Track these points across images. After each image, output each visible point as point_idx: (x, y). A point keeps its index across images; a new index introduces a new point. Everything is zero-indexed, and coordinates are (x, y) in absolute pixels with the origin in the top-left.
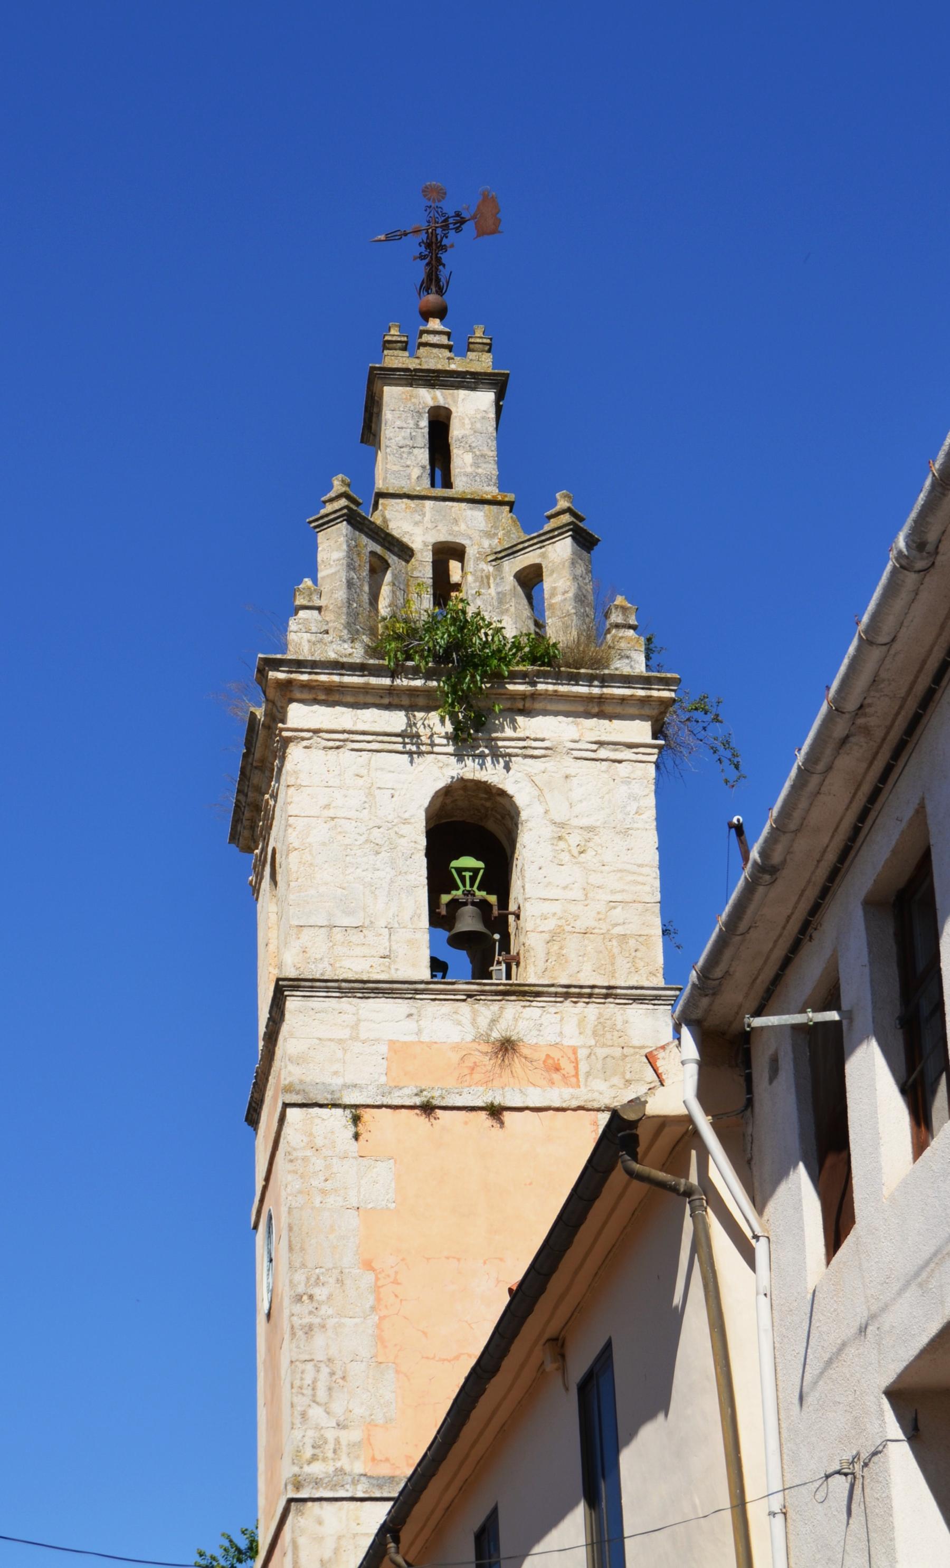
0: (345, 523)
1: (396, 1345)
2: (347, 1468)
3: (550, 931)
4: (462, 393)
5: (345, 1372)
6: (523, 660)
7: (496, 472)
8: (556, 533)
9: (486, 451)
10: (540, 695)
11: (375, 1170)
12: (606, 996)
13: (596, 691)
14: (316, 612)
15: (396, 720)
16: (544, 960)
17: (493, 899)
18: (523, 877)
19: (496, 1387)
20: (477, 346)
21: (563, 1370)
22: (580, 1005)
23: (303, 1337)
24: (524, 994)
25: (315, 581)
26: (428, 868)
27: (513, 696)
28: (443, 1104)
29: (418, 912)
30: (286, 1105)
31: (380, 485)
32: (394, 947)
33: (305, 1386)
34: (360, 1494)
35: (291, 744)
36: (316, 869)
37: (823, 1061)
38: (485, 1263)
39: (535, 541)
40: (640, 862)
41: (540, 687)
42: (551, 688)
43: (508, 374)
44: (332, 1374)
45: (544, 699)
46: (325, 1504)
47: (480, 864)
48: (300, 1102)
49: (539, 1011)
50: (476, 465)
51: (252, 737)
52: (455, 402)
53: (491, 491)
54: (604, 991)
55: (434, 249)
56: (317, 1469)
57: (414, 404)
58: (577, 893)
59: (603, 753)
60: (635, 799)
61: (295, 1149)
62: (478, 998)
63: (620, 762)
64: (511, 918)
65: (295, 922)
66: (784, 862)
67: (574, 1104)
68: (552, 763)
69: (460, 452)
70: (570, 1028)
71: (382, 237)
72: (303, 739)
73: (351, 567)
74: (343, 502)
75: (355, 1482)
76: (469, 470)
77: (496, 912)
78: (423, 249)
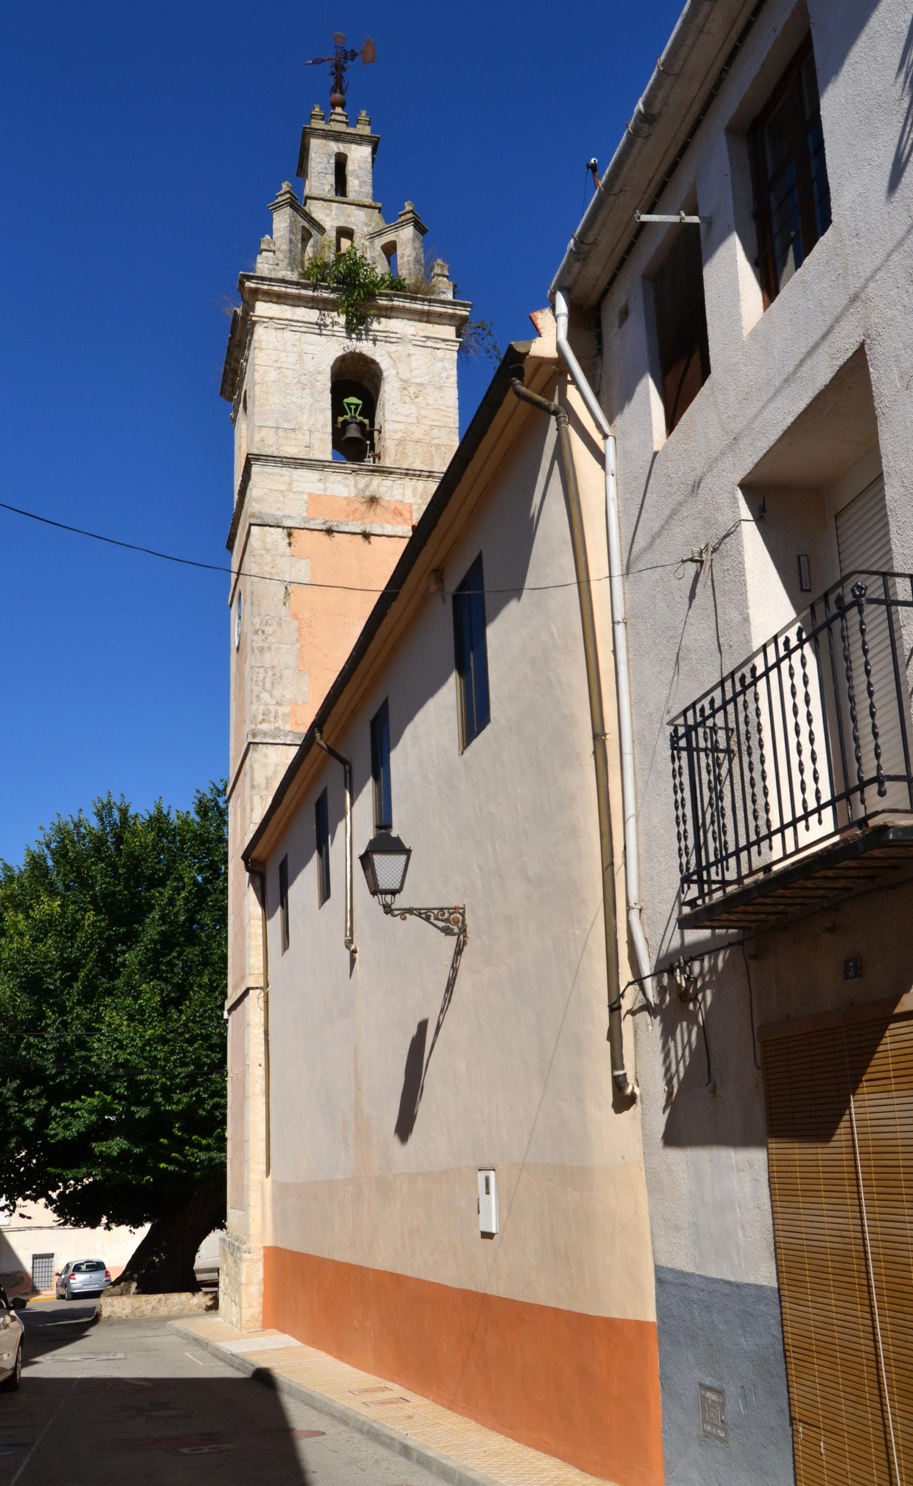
2: (282, 727)
4: (354, 146)
6: (386, 288)
7: (371, 191)
9: (366, 179)
12: (429, 477)
13: (426, 308)
14: (271, 254)
15: (313, 315)
17: (366, 421)
18: (384, 409)
19: (396, 607)
21: (441, 589)
23: (259, 654)
24: (383, 472)
25: (272, 237)
26: (133, 1256)
27: (381, 308)
28: (338, 530)
30: (251, 525)
31: (307, 192)
32: (313, 441)
34: (288, 742)
37: (686, 257)
41: (396, 303)
42: (401, 304)
43: (379, 138)
44: (274, 675)
46: (269, 746)
47: (360, 402)
49: (391, 483)
50: (361, 186)
52: (350, 150)
53: (368, 201)
55: (339, 70)
56: (265, 727)
58: (413, 420)
59: (429, 343)
64: (376, 433)
65: (257, 424)
66: (660, 113)
70: (409, 493)
73: (291, 232)
74: (288, 195)
75: (286, 735)
76: (357, 189)
77: (368, 428)
78: (333, 69)
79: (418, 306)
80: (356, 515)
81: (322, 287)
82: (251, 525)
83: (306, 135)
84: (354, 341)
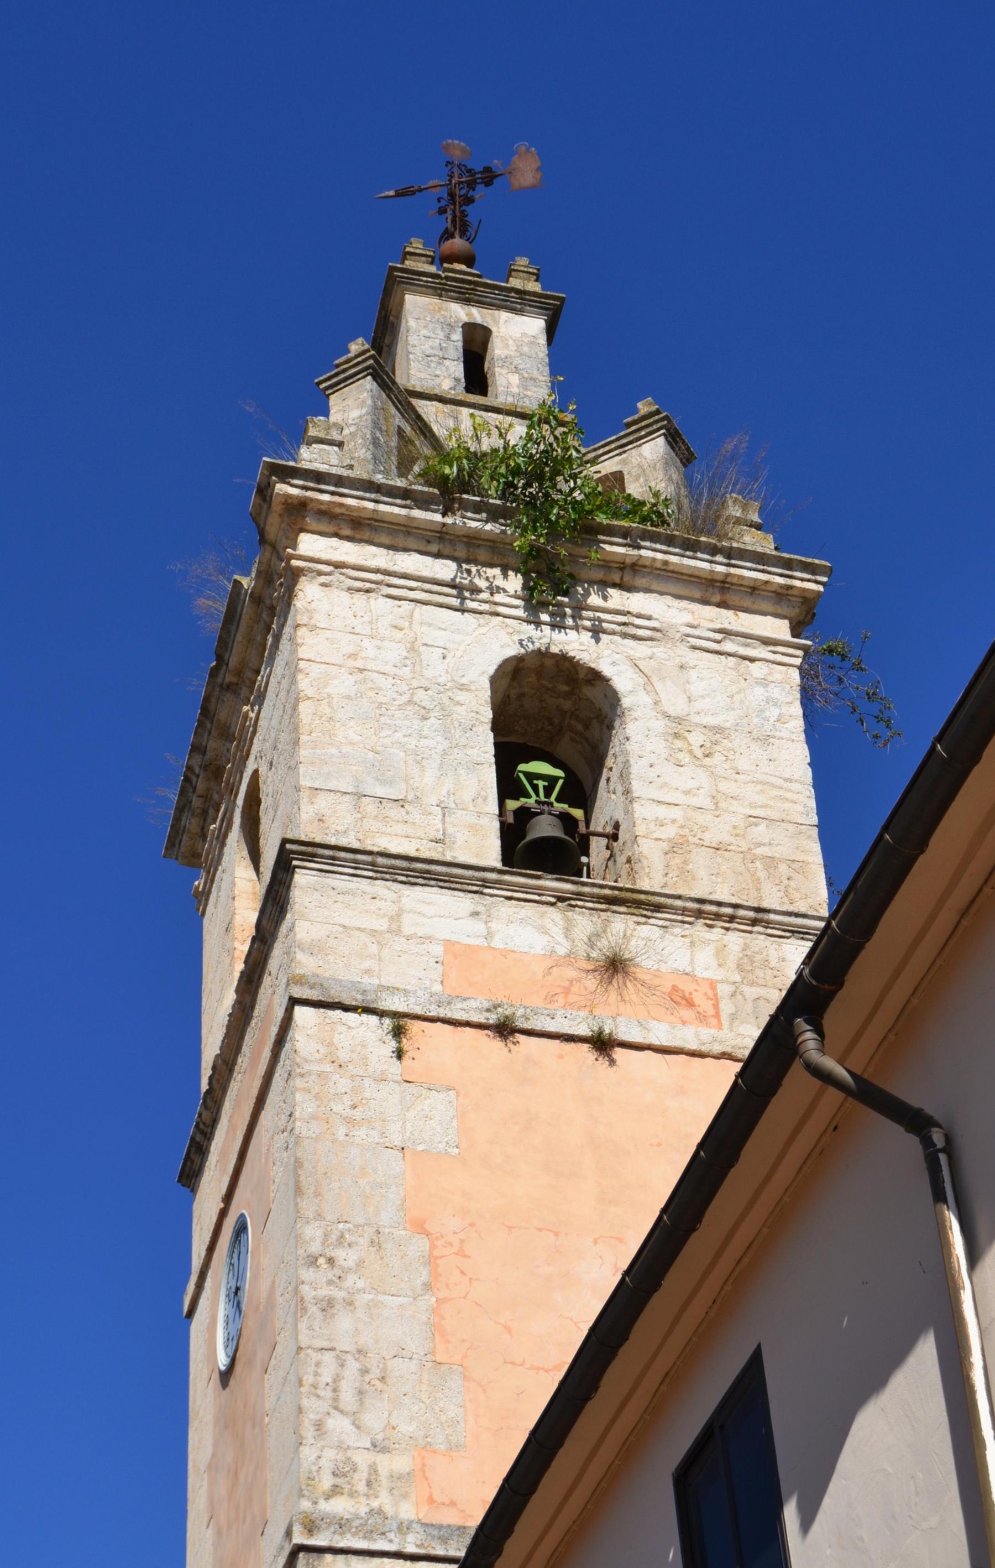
0: (369, 378)
1: (463, 1341)
2: (389, 1510)
3: (669, 840)
4: (504, 315)
5: (384, 1370)
8: (643, 433)
10: (644, 567)
11: (427, 1102)
12: (754, 922)
13: (721, 569)
14: (336, 448)
15: (445, 569)
16: (663, 872)
17: (578, 813)
20: (521, 274)
22: (718, 931)
23: (319, 1315)
24: (639, 904)
27: (607, 564)
28: (527, 1026)
29: (483, 793)
30: (294, 1002)
31: (301, 656)
32: (450, 830)
33: (322, 1385)
34: (411, 1549)
35: (302, 579)
36: (338, 725)
38: (596, 1242)
39: (613, 446)
40: (787, 776)
43: (562, 300)
44: (365, 1371)
45: (650, 573)
46: (354, 1559)
47: (559, 773)
48: (315, 998)
51: (229, 632)
52: (497, 322)
54: (751, 914)
56: (339, 1506)
57: (444, 317)
59: (729, 646)
60: (775, 704)
61: (306, 1061)
62: (573, 902)
63: (752, 660)
67: (717, 1049)
68: (661, 649)
69: (504, 371)
71: (392, 193)
72: (320, 573)
76: (515, 390)
79: (700, 564)
80: (572, 998)
81: (465, 506)
82: (294, 1002)
83: (393, 285)
84: (547, 629)
